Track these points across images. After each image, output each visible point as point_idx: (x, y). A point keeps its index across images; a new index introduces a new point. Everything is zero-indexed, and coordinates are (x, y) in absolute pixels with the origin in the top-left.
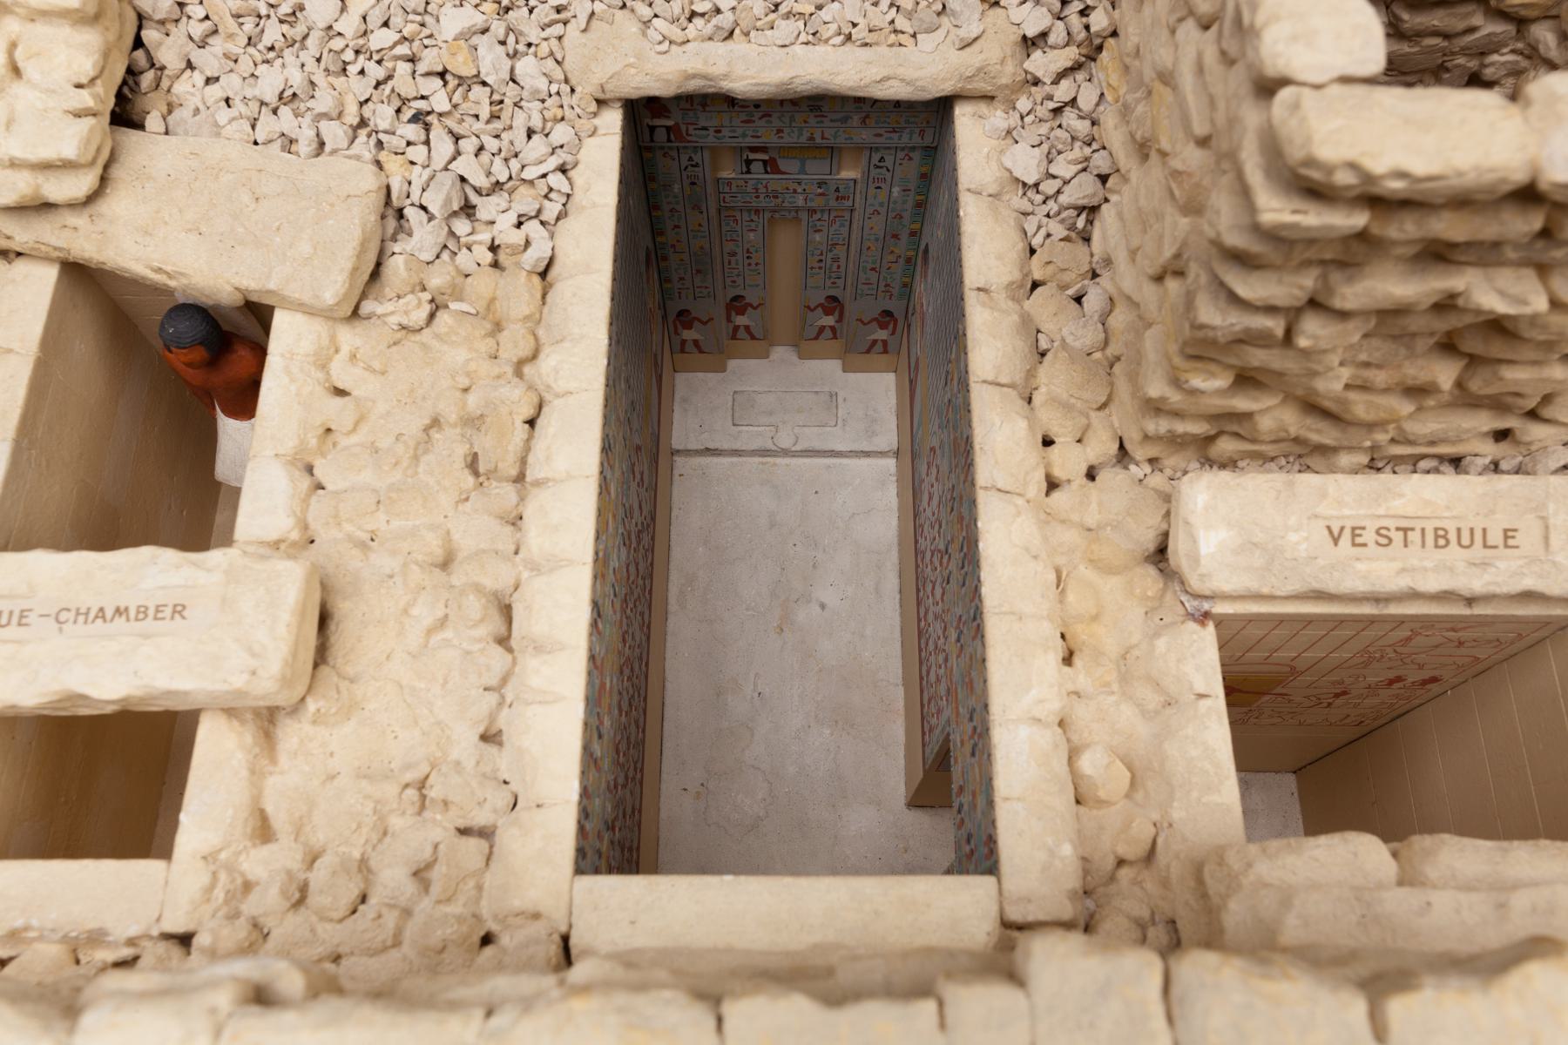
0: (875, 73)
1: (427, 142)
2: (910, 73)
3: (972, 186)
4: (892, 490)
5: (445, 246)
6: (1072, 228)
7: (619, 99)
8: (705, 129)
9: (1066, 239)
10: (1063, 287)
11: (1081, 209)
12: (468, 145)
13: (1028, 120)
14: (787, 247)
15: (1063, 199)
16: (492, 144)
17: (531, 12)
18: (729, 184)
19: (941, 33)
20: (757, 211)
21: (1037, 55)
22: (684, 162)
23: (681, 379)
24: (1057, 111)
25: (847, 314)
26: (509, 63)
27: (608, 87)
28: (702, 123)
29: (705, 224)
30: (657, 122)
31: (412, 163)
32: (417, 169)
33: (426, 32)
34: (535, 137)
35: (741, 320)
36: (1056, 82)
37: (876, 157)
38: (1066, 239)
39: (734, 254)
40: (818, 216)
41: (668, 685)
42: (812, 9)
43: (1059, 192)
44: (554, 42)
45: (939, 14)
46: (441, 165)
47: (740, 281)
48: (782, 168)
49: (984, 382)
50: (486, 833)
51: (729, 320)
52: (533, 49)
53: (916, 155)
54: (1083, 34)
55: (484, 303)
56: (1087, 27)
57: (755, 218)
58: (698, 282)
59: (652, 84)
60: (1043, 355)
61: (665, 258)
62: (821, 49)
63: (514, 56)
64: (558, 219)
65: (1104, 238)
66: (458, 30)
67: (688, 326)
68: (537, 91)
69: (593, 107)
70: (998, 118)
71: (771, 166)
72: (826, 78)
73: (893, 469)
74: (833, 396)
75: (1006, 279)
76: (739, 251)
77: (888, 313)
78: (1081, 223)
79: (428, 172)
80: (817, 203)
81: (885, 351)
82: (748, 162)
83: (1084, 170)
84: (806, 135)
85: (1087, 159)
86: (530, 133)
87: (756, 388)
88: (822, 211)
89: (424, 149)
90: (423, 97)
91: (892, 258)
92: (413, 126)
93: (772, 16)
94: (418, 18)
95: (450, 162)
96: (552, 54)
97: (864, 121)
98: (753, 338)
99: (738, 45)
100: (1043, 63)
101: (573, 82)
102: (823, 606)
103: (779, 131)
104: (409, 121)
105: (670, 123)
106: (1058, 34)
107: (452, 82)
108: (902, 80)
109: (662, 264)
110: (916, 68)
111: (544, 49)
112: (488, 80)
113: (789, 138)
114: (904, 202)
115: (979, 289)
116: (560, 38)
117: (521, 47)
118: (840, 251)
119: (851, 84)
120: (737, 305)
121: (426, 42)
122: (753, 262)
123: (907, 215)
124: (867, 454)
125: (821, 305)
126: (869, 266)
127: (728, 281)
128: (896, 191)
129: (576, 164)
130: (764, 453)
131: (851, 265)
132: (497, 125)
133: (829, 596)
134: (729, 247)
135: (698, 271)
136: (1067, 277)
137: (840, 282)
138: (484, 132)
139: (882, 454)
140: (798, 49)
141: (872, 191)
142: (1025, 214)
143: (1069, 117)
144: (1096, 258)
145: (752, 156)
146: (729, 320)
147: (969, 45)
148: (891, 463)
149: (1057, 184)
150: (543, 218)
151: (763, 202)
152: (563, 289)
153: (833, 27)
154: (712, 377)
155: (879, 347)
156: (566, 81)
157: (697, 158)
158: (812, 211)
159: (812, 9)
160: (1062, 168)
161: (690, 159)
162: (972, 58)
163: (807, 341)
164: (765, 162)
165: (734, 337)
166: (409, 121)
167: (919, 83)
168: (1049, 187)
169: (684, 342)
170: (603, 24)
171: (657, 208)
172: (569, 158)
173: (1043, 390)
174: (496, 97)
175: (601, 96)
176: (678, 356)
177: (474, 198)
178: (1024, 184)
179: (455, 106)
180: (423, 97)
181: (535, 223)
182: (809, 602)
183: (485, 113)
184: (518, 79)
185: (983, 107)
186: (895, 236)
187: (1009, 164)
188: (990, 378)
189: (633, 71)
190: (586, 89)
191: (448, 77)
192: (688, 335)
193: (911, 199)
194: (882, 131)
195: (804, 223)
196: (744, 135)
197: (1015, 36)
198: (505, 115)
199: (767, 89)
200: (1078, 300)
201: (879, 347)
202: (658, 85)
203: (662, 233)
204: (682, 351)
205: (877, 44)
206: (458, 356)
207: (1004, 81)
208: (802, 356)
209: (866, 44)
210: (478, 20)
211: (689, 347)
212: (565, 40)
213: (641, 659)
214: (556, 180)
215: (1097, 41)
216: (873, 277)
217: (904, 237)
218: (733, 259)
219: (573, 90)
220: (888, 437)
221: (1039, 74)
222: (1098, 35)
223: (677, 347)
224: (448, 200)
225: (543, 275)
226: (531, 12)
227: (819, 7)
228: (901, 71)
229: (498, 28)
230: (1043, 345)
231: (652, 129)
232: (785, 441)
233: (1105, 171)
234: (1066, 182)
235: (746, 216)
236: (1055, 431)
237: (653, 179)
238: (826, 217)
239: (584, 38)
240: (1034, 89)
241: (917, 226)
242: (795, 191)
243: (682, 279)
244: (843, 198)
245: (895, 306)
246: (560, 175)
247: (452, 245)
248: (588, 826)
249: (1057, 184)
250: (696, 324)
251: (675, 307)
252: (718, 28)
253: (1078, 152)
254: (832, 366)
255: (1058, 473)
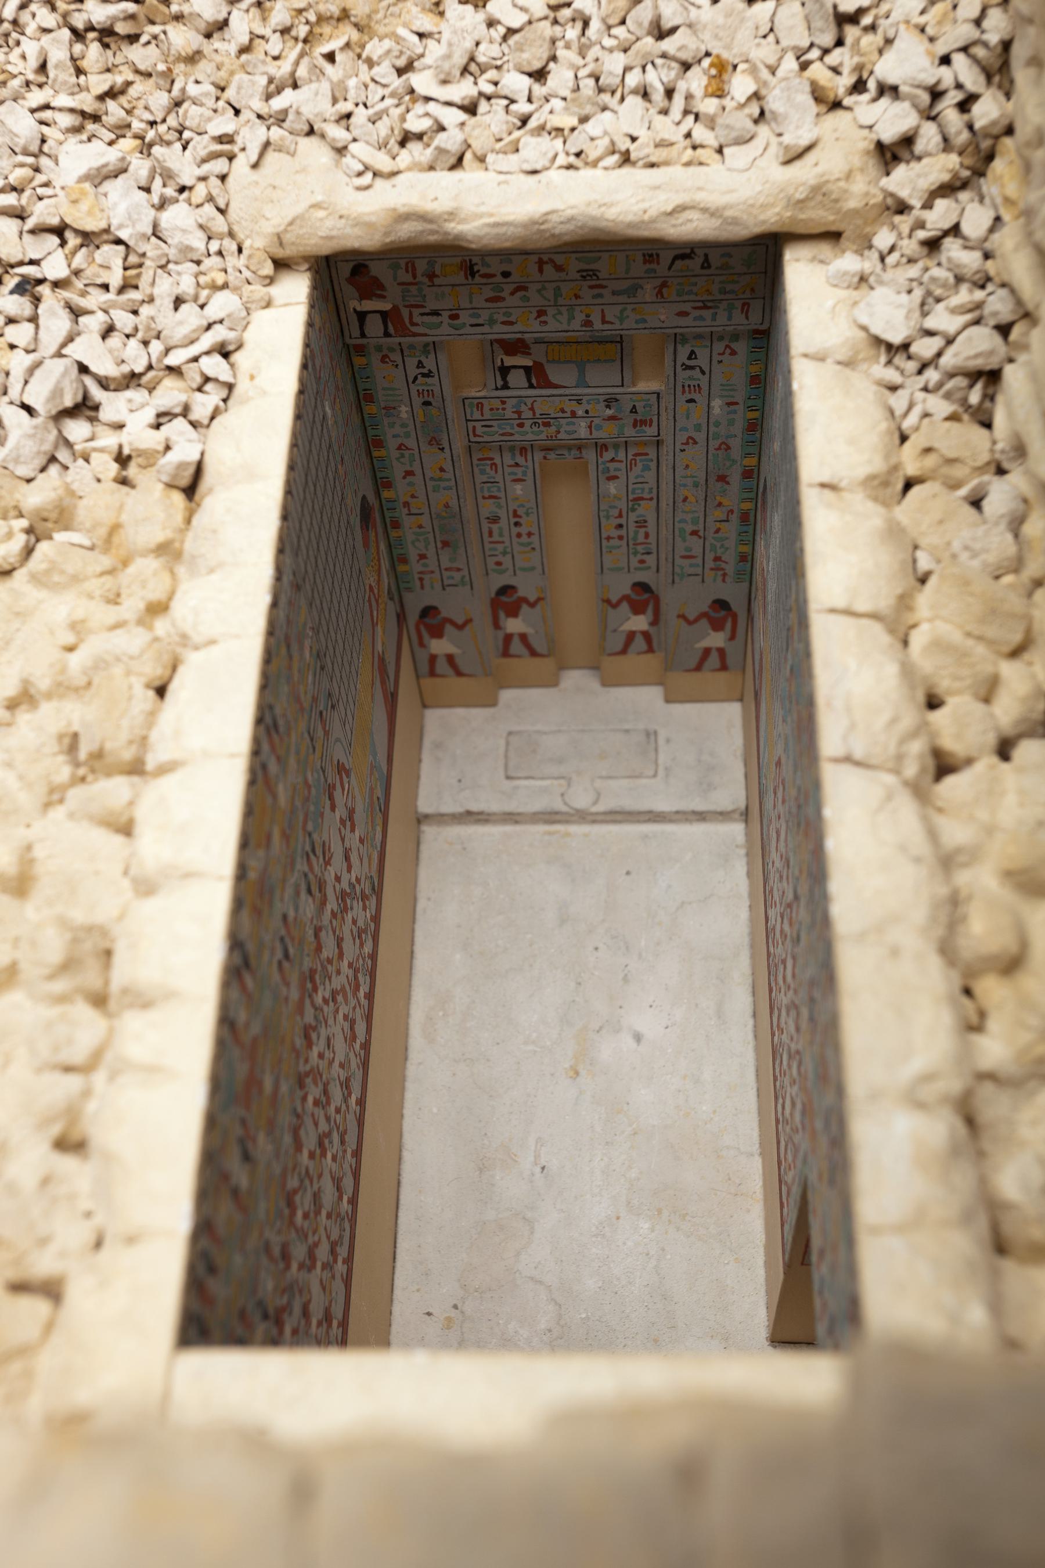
0: (664, 201)
1: (34, 319)
2: (713, 199)
3: (811, 350)
4: (740, 868)
5: (53, 459)
6: (964, 402)
7: (306, 258)
8: (436, 313)
9: (953, 417)
10: (955, 486)
11: (974, 376)
12: (93, 323)
13: (891, 260)
14: (570, 516)
15: (948, 360)
16: (123, 320)
17: (185, 148)
18: (480, 406)
19: (758, 144)
20: (523, 451)
21: (901, 172)
22: (413, 371)
23: (433, 717)
24: (933, 245)
25: (663, 607)
26: (153, 212)
27: (288, 238)
28: (431, 305)
29: (448, 466)
30: (368, 305)
31: (12, 347)
32: (19, 353)
33: (40, 178)
34: (184, 307)
35: (514, 625)
36: (928, 205)
37: (683, 352)
38: (953, 417)
39: (495, 520)
40: (608, 455)
41: (406, 1155)
42: (574, 121)
43: (939, 354)
44: (214, 182)
45: (756, 122)
46: (53, 349)
47: (507, 561)
48: (554, 379)
49: (833, 611)
50: (51, 1290)
51: (497, 625)
52: (185, 195)
53: (741, 347)
54: (965, 135)
55: (103, 531)
56: (970, 127)
57: (520, 460)
58: (445, 563)
59: (348, 230)
60: (923, 580)
61: (396, 525)
62: (586, 174)
63: (162, 205)
64: (212, 418)
65: (1011, 415)
66: (82, 170)
67: (437, 632)
68: (189, 249)
69: (268, 269)
70: (849, 262)
71: (536, 376)
72: (595, 211)
73: (741, 838)
74: (651, 735)
75: (862, 471)
76: (502, 514)
77: (721, 604)
78: (975, 397)
79: (32, 357)
80: (606, 432)
81: (724, 667)
82: (505, 371)
83: (977, 322)
84: (580, 317)
85: (979, 306)
86: (178, 302)
87: (539, 727)
88: (616, 446)
89: (30, 327)
90: (32, 262)
91: (719, 514)
92: (16, 297)
93: (517, 134)
94: (30, 160)
95: (64, 345)
96: (210, 199)
97: (660, 293)
98: (533, 653)
99: (470, 175)
100: (907, 180)
101: (241, 236)
102: (638, 1038)
103: (541, 313)
104: (12, 292)
105: (386, 306)
106: (929, 136)
107: (73, 241)
108: (704, 210)
109: (393, 534)
110: (727, 188)
111: (200, 191)
112: (123, 235)
113: (556, 325)
114: (731, 423)
115: (823, 485)
116: (223, 178)
117: (170, 192)
118: (646, 510)
119: (630, 218)
120: (506, 601)
121: (40, 191)
122: (523, 530)
123: (736, 444)
124: (701, 816)
125: (625, 598)
126: (689, 528)
127: (491, 562)
128: (717, 403)
129: (240, 347)
130: (550, 817)
131: (663, 532)
132: (133, 295)
133: (648, 1023)
134: (488, 508)
135: (446, 544)
136: (958, 472)
137: (651, 560)
138: (114, 305)
139: (723, 816)
140: (555, 175)
141: (682, 405)
142: (893, 388)
143: (952, 248)
144: (1000, 446)
145: (509, 361)
146: (497, 625)
147: (800, 156)
148: (736, 830)
149: (936, 343)
150: (194, 416)
151: (529, 434)
152: (215, 501)
153: (603, 144)
154: (478, 714)
155: (714, 660)
156: (231, 234)
157: (429, 363)
158: (601, 447)
159: (574, 121)
160: (942, 319)
161: (420, 364)
162: (804, 172)
163: (613, 657)
164: (527, 370)
165: (506, 653)
166: (12, 292)
167: (728, 213)
168: (925, 348)
169: (433, 659)
170: (282, 156)
171: (379, 444)
172: (231, 335)
173: (925, 627)
174: (133, 259)
175: (280, 253)
176: (427, 682)
177: (97, 393)
178: (889, 347)
179: (77, 273)
180: (32, 262)
181: (180, 423)
182: (618, 1031)
183: (115, 279)
184: (164, 234)
185: (824, 249)
186: (722, 479)
187: (864, 320)
188: (841, 603)
189: (321, 214)
190: (256, 242)
191: (69, 235)
192: (440, 646)
193: (741, 417)
194: (687, 307)
195: (592, 468)
196: (492, 322)
197: (864, 142)
198: (144, 282)
199: (511, 230)
200: (976, 503)
201: (714, 660)
202: (357, 231)
203: (388, 485)
204: (432, 673)
205: (667, 163)
206: (59, 609)
207: (852, 204)
208: (605, 683)
209: (652, 165)
210: (111, 156)
211: (442, 666)
212: (230, 179)
213: (346, 1085)
214: (214, 365)
215: (986, 144)
216: (696, 544)
217: (735, 478)
218: (495, 527)
219: (240, 250)
220: (732, 792)
221: (904, 194)
222: (987, 136)
223: (424, 668)
224: (57, 392)
225: (190, 491)
226: (185, 148)
227: (584, 120)
228: (701, 197)
229: (140, 167)
230: (924, 562)
231: (362, 316)
232: (581, 800)
233: (1006, 317)
234: (950, 341)
235: (508, 460)
236: (944, 685)
237: (370, 398)
238: (621, 455)
239: (254, 176)
240: (897, 219)
241: (753, 461)
242: (573, 414)
243: (422, 557)
244: (643, 422)
245: (732, 593)
246: (217, 358)
247: (63, 455)
248: (216, 1287)
249: (936, 343)
250: (449, 628)
251: (414, 605)
252: (441, 151)
253: (964, 295)
254: (650, 696)
255: (949, 743)
